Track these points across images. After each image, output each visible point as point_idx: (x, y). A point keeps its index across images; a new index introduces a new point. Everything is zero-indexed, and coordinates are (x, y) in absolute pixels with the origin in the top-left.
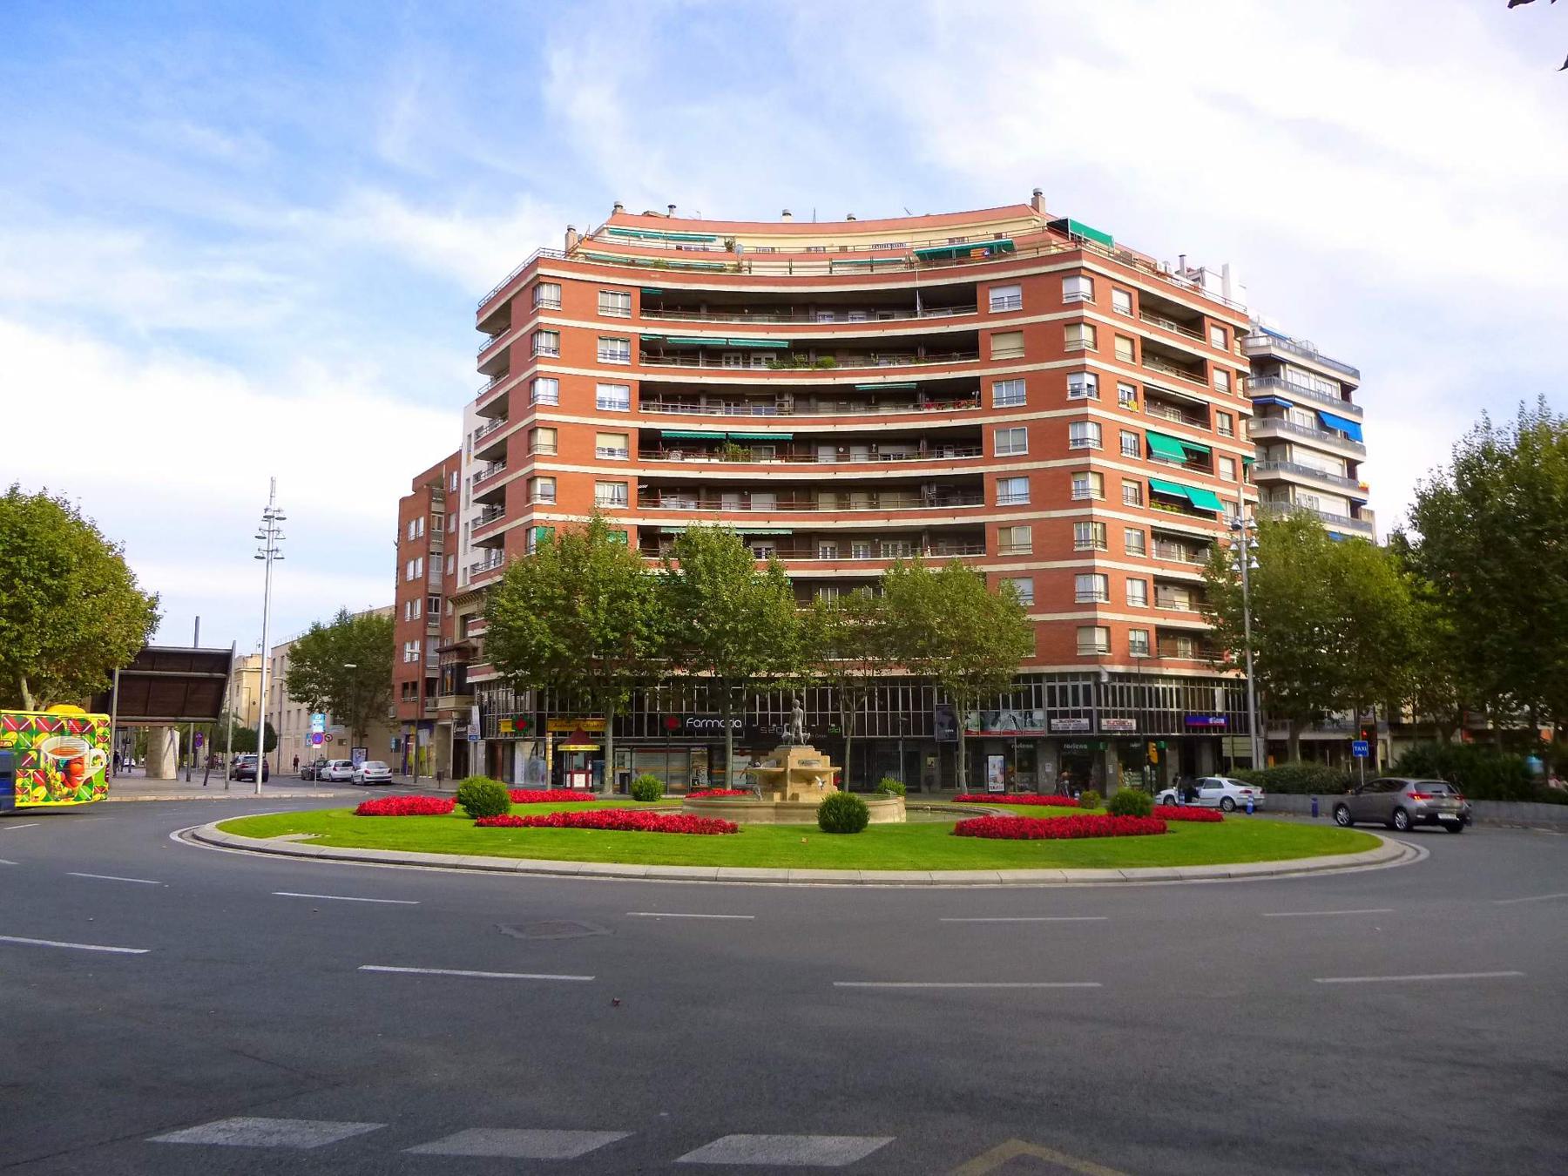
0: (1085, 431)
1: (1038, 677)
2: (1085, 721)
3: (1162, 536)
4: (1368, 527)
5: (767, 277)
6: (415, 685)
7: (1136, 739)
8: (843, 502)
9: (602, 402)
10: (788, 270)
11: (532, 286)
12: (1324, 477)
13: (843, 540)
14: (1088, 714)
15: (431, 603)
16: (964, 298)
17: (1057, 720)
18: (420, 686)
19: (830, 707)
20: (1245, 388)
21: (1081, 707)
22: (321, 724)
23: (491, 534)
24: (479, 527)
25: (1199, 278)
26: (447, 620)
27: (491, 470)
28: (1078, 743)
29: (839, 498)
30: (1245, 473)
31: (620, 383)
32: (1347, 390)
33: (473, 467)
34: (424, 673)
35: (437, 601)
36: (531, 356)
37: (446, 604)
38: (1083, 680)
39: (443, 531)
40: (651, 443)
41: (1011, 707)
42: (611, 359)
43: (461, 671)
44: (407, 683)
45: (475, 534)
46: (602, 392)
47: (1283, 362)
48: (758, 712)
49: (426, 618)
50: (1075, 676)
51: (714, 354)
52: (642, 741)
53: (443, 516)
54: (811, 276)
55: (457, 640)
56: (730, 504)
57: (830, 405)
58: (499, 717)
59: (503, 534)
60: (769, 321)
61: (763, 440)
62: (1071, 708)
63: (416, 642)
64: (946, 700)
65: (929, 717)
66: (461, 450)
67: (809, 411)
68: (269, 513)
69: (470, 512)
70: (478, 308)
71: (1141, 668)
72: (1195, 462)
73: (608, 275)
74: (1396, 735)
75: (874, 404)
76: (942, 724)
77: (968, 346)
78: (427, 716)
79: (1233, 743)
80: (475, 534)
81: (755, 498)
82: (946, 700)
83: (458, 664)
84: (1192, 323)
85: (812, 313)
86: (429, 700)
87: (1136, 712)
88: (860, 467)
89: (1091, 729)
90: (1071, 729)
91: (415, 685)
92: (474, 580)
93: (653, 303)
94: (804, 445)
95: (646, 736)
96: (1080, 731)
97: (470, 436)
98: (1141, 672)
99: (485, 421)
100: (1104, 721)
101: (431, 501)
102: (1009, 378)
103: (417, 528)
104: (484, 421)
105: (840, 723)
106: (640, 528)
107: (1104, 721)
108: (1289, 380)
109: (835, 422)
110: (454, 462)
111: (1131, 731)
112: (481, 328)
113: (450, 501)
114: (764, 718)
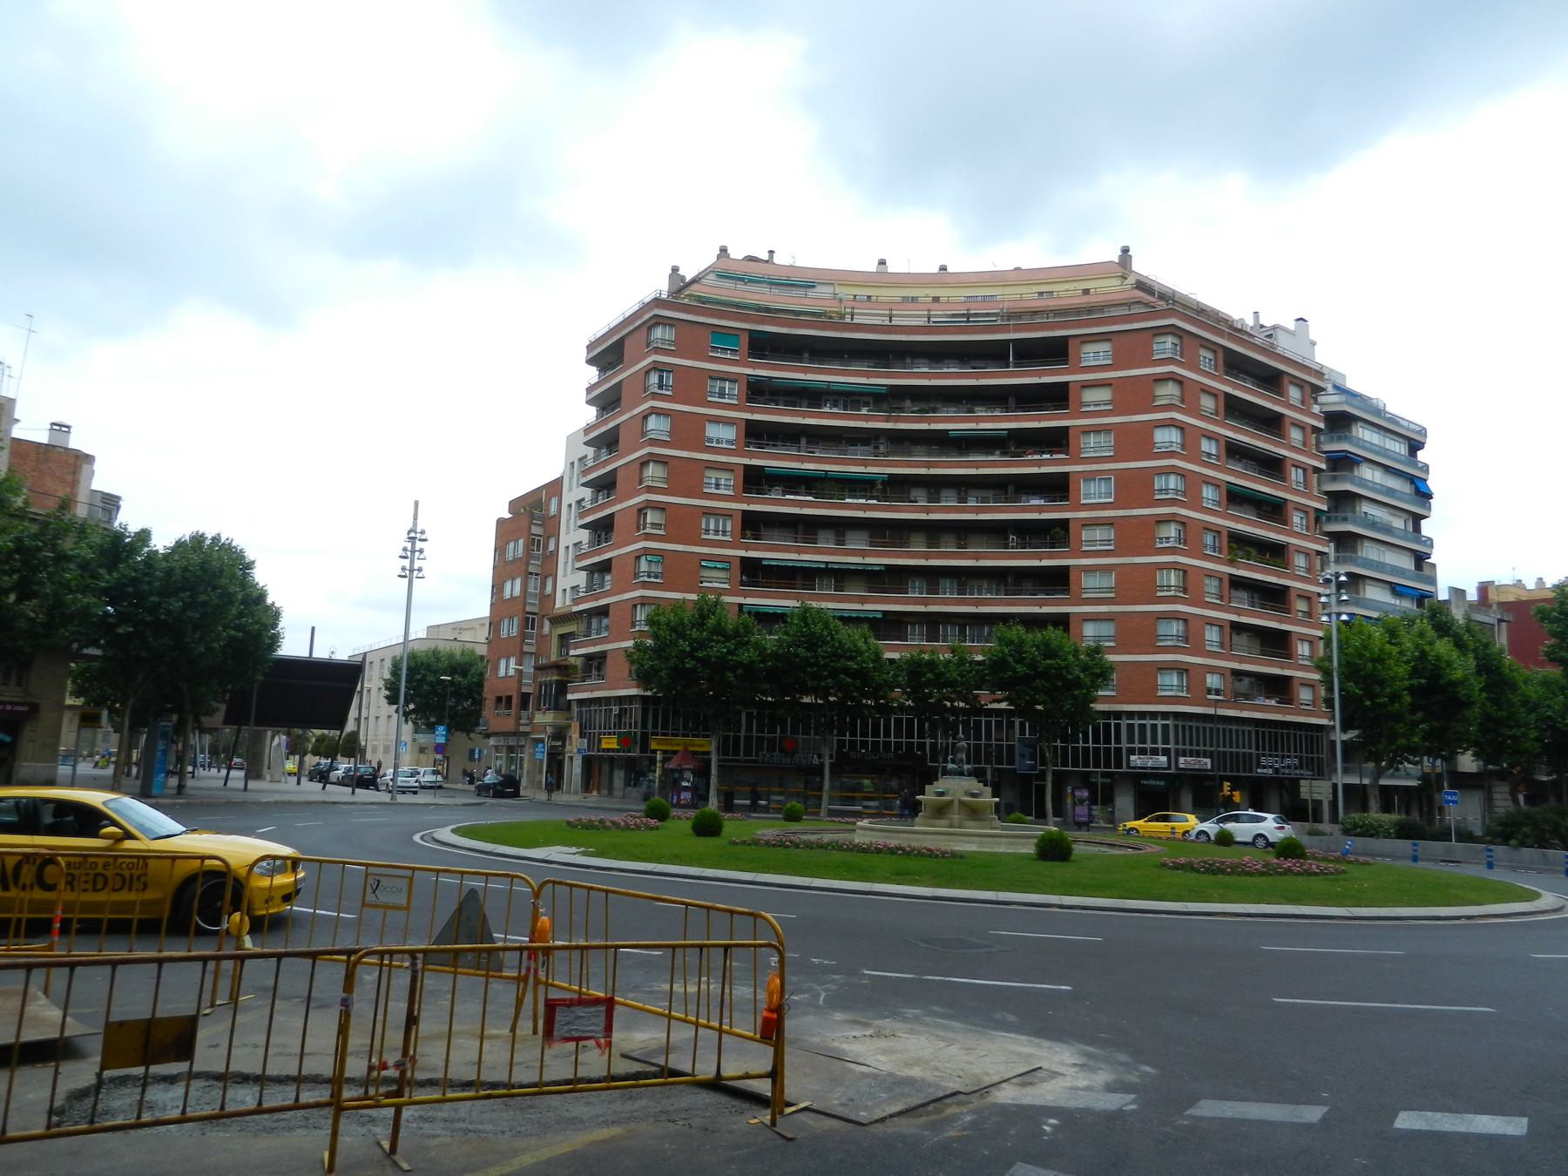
0: (1167, 482)
1: (1118, 715)
2: (1164, 759)
3: (1237, 583)
4: (1432, 580)
5: (869, 321)
6: (509, 699)
7: (1213, 778)
8: (933, 542)
9: (710, 440)
10: (888, 318)
11: (648, 325)
12: (1388, 529)
13: (932, 577)
14: (1166, 752)
15: (528, 622)
16: (1055, 351)
17: (1136, 757)
18: (514, 701)
19: (1113, 740)
20: (1318, 443)
21: (1160, 746)
22: (443, 735)
23: (597, 559)
24: (583, 551)
25: (1271, 335)
26: (543, 638)
27: (595, 500)
28: (1155, 779)
29: (959, 538)
30: (1316, 526)
31: (728, 422)
32: (1415, 446)
33: (576, 493)
34: (520, 688)
35: (533, 620)
36: (645, 392)
37: (543, 621)
38: (1162, 720)
39: (541, 552)
40: (755, 480)
41: (252, 721)
42: (729, 399)
43: (562, 688)
44: (502, 697)
45: (578, 558)
46: (713, 431)
47: (1356, 419)
48: (916, 740)
49: (523, 636)
50: (1154, 715)
51: (813, 396)
52: (737, 761)
53: (541, 539)
54: (911, 323)
55: (554, 658)
56: (826, 541)
57: (924, 448)
58: (600, 734)
59: (610, 559)
60: (869, 367)
61: (860, 480)
62: (1149, 745)
63: (512, 659)
64: (1027, 733)
65: (1011, 749)
66: (562, 477)
67: (903, 454)
68: (413, 535)
69: (572, 535)
70: (588, 343)
71: (1218, 710)
72: (1271, 513)
73: (720, 318)
74: (596, 786)
75: (965, 449)
76: (1022, 756)
77: (1057, 396)
78: (522, 729)
79: (1311, 786)
80: (578, 558)
81: (850, 535)
82: (1027, 733)
83: (558, 682)
84: (1271, 379)
85: (908, 361)
86: (524, 713)
87: (1211, 752)
88: (973, 511)
89: (1169, 768)
90: (1149, 765)
91: (509, 699)
92: (576, 601)
93: (762, 346)
94: (897, 487)
95: (742, 757)
96: (1158, 768)
97: (573, 463)
98: (1218, 713)
99: (590, 451)
100: (1182, 760)
101: (531, 523)
102: (1097, 430)
103: (517, 549)
104: (590, 451)
105: (925, 750)
106: (743, 559)
107: (1182, 760)
108: (1361, 436)
109: (928, 465)
110: (555, 487)
111: (1206, 770)
112: (590, 362)
113: (551, 526)
114: (853, 744)
